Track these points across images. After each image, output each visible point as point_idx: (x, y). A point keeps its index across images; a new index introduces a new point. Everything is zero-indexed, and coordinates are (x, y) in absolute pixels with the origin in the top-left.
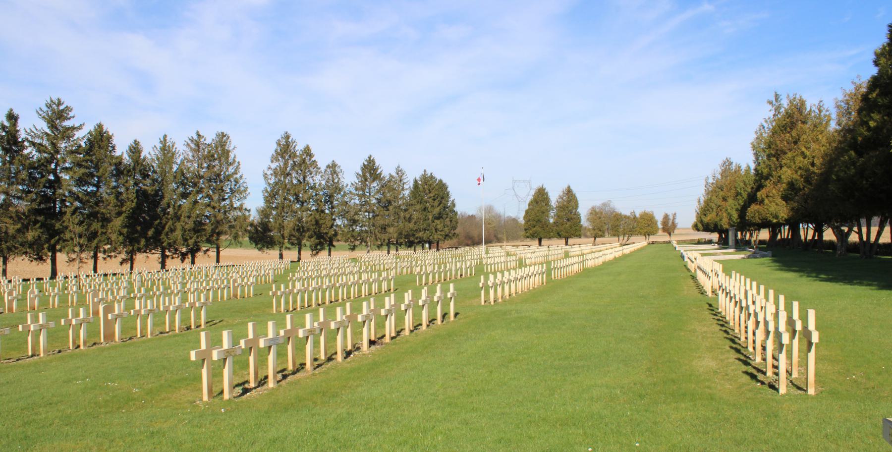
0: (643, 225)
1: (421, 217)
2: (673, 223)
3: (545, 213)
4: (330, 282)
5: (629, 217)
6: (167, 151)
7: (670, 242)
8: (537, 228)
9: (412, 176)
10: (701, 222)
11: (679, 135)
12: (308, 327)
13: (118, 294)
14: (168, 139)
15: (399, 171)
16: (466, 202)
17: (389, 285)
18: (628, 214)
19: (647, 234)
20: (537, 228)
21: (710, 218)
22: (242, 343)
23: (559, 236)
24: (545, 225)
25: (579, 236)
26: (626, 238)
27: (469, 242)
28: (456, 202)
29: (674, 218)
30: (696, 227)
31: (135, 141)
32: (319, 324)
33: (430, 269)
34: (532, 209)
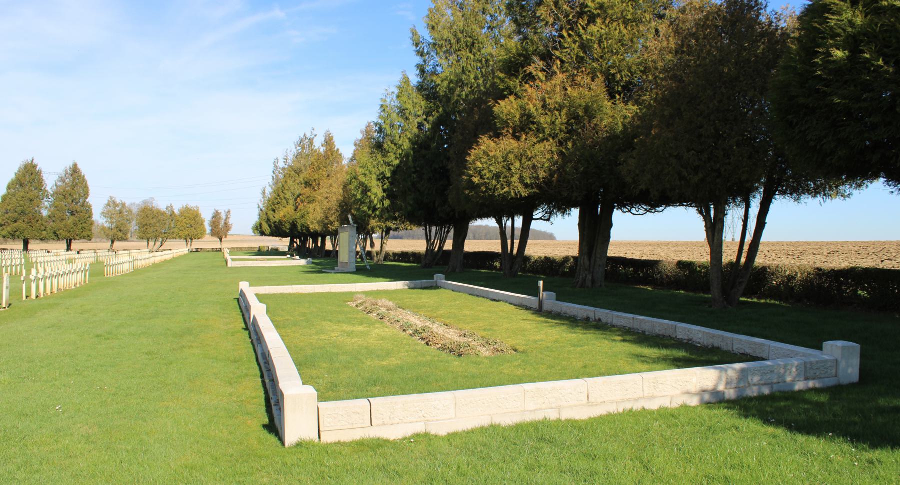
0: (186, 225)
2: (225, 223)
5: (163, 213)
7: (220, 250)
10: (268, 220)
19: (189, 238)
21: (285, 213)
23: (57, 237)
24: (35, 218)
25: (89, 238)
26: (158, 244)
29: (227, 218)
30: (259, 230)
33: (18, 262)
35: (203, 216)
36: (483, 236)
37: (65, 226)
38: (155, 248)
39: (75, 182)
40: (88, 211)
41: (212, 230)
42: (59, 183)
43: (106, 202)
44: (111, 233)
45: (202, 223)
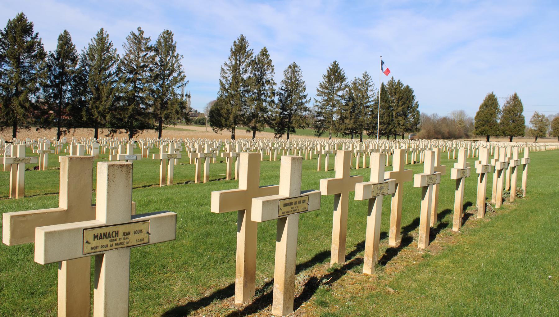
1: (395, 113)
3: (493, 114)
6: (102, 43)
8: (486, 127)
9: (378, 82)
12: (374, 179)
14: (104, 32)
16: (431, 104)
20: (486, 127)
22: (323, 187)
23: (504, 134)
24: (493, 125)
25: (523, 135)
28: (419, 103)
31: (65, 31)
32: (392, 175)
34: (483, 112)
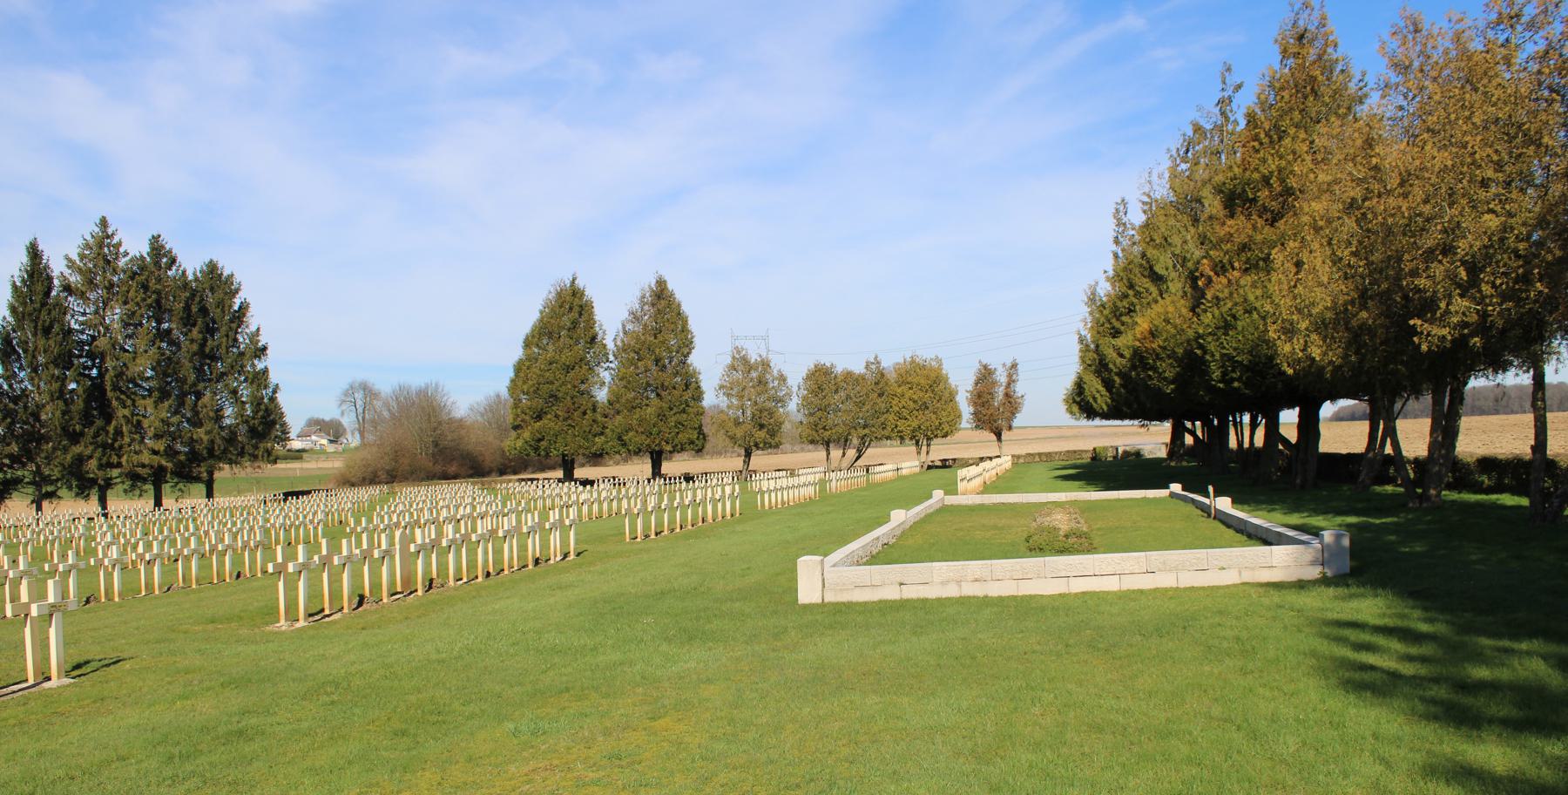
2: (1007, 395)
4: (457, 530)
11: (1002, 254)
13: (105, 555)
15: (157, 247)
17: (565, 541)
18: (858, 368)
19: (921, 437)
25: (698, 446)
27: (452, 469)
29: (1011, 381)
35: (954, 380)
36: (1246, 433)
37: (641, 421)
38: (845, 463)
39: (663, 315)
40: (691, 385)
41: (975, 414)
42: (629, 327)
43: (729, 360)
44: (739, 432)
45: (952, 398)
